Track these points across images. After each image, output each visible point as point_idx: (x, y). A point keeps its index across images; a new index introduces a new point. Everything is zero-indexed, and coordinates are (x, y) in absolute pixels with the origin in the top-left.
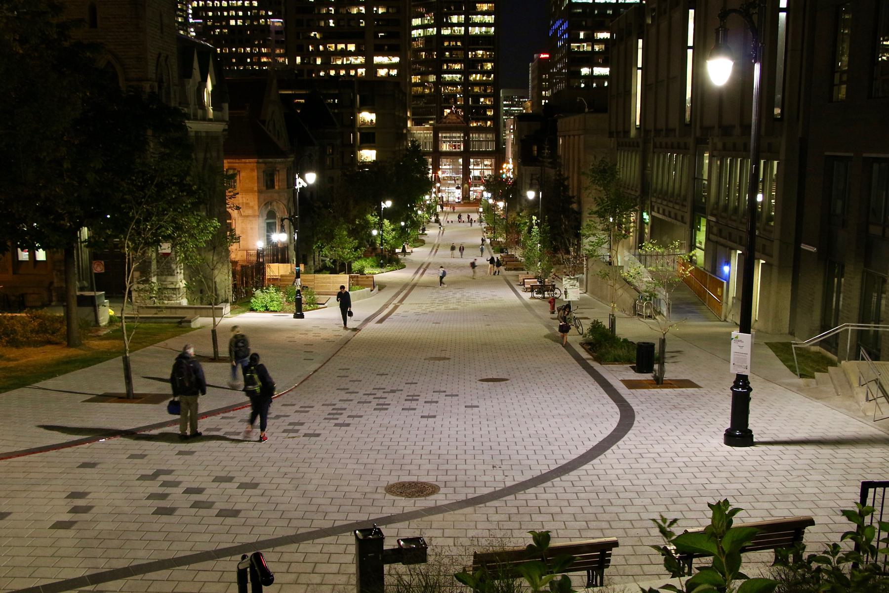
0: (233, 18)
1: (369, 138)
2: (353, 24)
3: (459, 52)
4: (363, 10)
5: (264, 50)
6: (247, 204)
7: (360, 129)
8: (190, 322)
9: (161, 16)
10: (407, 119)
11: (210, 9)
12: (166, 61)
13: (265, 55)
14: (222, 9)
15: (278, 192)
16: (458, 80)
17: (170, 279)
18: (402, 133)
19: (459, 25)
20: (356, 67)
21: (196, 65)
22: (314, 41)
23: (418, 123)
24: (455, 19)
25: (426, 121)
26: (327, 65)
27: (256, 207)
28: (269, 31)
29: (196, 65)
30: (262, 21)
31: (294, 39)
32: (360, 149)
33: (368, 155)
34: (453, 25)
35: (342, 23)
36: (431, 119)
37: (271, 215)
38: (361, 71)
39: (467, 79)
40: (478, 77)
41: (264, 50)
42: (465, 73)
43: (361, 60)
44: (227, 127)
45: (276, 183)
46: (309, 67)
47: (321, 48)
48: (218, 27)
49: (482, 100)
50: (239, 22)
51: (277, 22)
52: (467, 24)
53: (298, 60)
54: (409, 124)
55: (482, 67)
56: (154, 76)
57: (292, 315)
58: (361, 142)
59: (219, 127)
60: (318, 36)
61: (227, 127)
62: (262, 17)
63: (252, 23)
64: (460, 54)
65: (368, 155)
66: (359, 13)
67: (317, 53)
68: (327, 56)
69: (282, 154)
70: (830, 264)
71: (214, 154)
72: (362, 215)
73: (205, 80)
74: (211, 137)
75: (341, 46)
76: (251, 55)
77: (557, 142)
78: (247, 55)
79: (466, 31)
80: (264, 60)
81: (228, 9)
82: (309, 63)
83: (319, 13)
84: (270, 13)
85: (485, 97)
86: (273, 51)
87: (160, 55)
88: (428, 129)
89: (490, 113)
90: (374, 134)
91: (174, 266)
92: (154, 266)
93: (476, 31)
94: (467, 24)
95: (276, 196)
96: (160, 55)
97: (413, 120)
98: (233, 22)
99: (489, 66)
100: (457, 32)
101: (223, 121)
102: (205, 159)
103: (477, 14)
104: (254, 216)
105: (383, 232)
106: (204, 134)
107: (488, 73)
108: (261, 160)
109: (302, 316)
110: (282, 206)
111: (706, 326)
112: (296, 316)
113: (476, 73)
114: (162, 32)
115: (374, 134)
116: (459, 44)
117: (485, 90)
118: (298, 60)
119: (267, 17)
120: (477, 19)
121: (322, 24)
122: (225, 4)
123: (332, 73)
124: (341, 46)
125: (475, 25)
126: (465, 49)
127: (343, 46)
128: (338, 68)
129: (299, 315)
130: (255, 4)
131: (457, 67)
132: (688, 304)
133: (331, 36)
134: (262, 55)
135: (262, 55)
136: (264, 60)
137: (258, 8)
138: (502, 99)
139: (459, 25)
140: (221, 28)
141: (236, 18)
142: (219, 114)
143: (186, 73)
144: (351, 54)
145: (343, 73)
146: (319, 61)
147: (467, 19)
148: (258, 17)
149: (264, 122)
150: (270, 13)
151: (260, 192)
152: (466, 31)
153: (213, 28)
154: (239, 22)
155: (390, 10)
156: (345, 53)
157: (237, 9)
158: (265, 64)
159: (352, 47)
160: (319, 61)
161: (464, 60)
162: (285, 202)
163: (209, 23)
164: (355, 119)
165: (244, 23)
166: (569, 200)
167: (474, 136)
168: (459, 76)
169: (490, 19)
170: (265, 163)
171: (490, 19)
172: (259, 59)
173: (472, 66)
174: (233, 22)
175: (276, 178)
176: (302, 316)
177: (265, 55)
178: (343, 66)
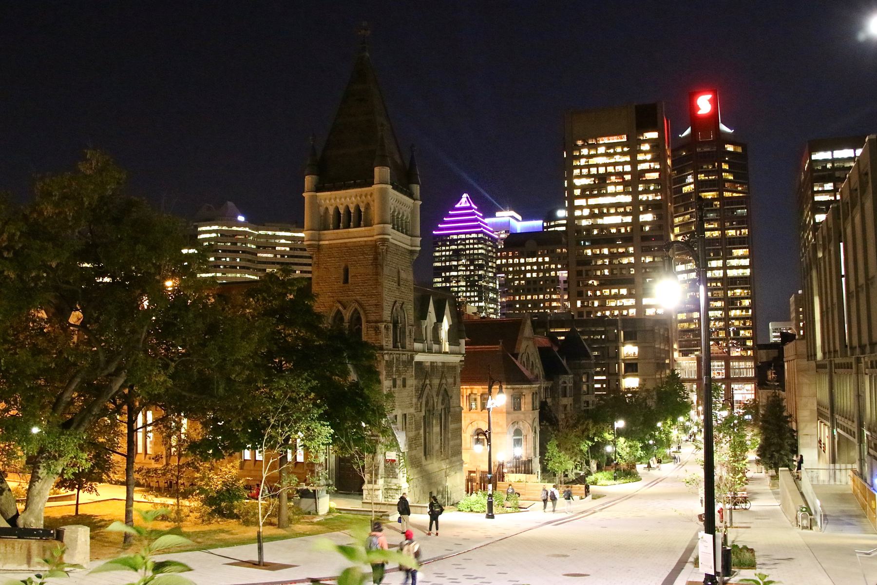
0: (529, 271)
1: (632, 367)
2: (624, 272)
3: (719, 292)
4: (632, 260)
5: (554, 297)
6: (497, 423)
7: (624, 360)
8: (388, 515)
9: (399, 272)
10: (673, 350)
11: (511, 265)
12: (401, 308)
13: (555, 300)
14: (520, 265)
15: (524, 414)
16: (719, 316)
17: (394, 481)
18: (664, 363)
19: (718, 268)
20: (627, 308)
21: (431, 308)
22: (594, 289)
23: (685, 354)
24: (714, 264)
25: (692, 352)
26: (603, 307)
27: (505, 426)
28: (558, 281)
29: (431, 308)
30: (553, 274)
31: (576, 288)
32: (624, 377)
33: (631, 382)
34: (712, 269)
35: (615, 272)
36: (697, 350)
37: (518, 432)
38: (632, 312)
39: (727, 314)
40: (738, 313)
41: (554, 297)
42: (726, 309)
43: (631, 302)
44: (463, 359)
45: (523, 406)
46: (588, 310)
47: (598, 293)
48: (517, 279)
49: (742, 332)
50: (535, 275)
51: (563, 274)
52: (725, 267)
53: (579, 304)
54: (676, 355)
55: (741, 303)
56: (389, 319)
57: (484, 515)
58: (625, 372)
59: (456, 359)
60: (596, 283)
61: (463, 359)
62: (553, 270)
63: (544, 274)
64: (721, 294)
65: (631, 382)
66: (603, 264)
67: (595, 297)
68: (603, 299)
69: (525, 380)
70: (776, 466)
71: (450, 380)
72: (599, 433)
73: (440, 319)
74: (451, 368)
75: (614, 291)
76: (544, 301)
77: (783, 366)
78: (540, 301)
79: (725, 274)
80: (554, 304)
81: (526, 264)
82: (588, 306)
83: (596, 265)
84: (559, 266)
85: (744, 329)
86: (562, 296)
87: (395, 302)
88: (692, 359)
89: (749, 343)
90: (636, 364)
91: (397, 471)
92: (381, 470)
93: (731, 273)
94: (725, 267)
95: (522, 416)
96: (395, 302)
97: (680, 351)
98: (528, 275)
99: (746, 303)
100: (717, 275)
101: (460, 354)
102: (440, 385)
103: (734, 258)
104: (503, 433)
105: (621, 448)
106: (429, 364)
107: (746, 309)
108: (509, 387)
109: (492, 517)
110: (527, 425)
111: (856, 538)
112: (488, 517)
113: (736, 309)
114: (399, 285)
115: (636, 364)
116: (719, 284)
117: (744, 324)
118: (579, 304)
119: (556, 270)
120: (734, 262)
121: (599, 273)
122: (522, 261)
123: (608, 313)
124: (614, 291)
125: (732, 268)
126: (725, 289)
127: (616, 291)
128: (611, 309)
129: (491, 516)
130: (547, 259)
131: (719, 304)
132: (851, 516)
133: (606, 282)
134: (551, 300)
135: (551, 300)
136: (554, 304)
137: (550, 263)
138: (771, 331)
139: (718, 268)
140: (520, 279)
141: (532, 271)
142: (455, 348)
143: (422, 314)
144: (623, 297)
145: (616, 313)
146: (596, 304)
147: (724, 264)
148: (549, 270)
149: (516, 356)
150: (559, 266)
151: (508, 413)
152: (725, 274)
153: (513, 280)
154: (535, 275)
155: (656, 259)
156: (617, 297)
157: (532, 264)
158: (556, 308)
159: (624, 291)
160: (596, 304)
161: (725, 299)
162: (530, 422)
163: (510, 277)
164: (617, 354)
165: (538, 275)
166: (785, 420)
167: (734, 364)
168: (721, 312)
169: (746, 262)
170: (513, 389)
171: (746, 262)
172: (550, 304)
173: (731, 303)
174: (528, 275)
175: (523, 401)
176: (492, 517)
177: (555, 300)
178: (616, 308)
